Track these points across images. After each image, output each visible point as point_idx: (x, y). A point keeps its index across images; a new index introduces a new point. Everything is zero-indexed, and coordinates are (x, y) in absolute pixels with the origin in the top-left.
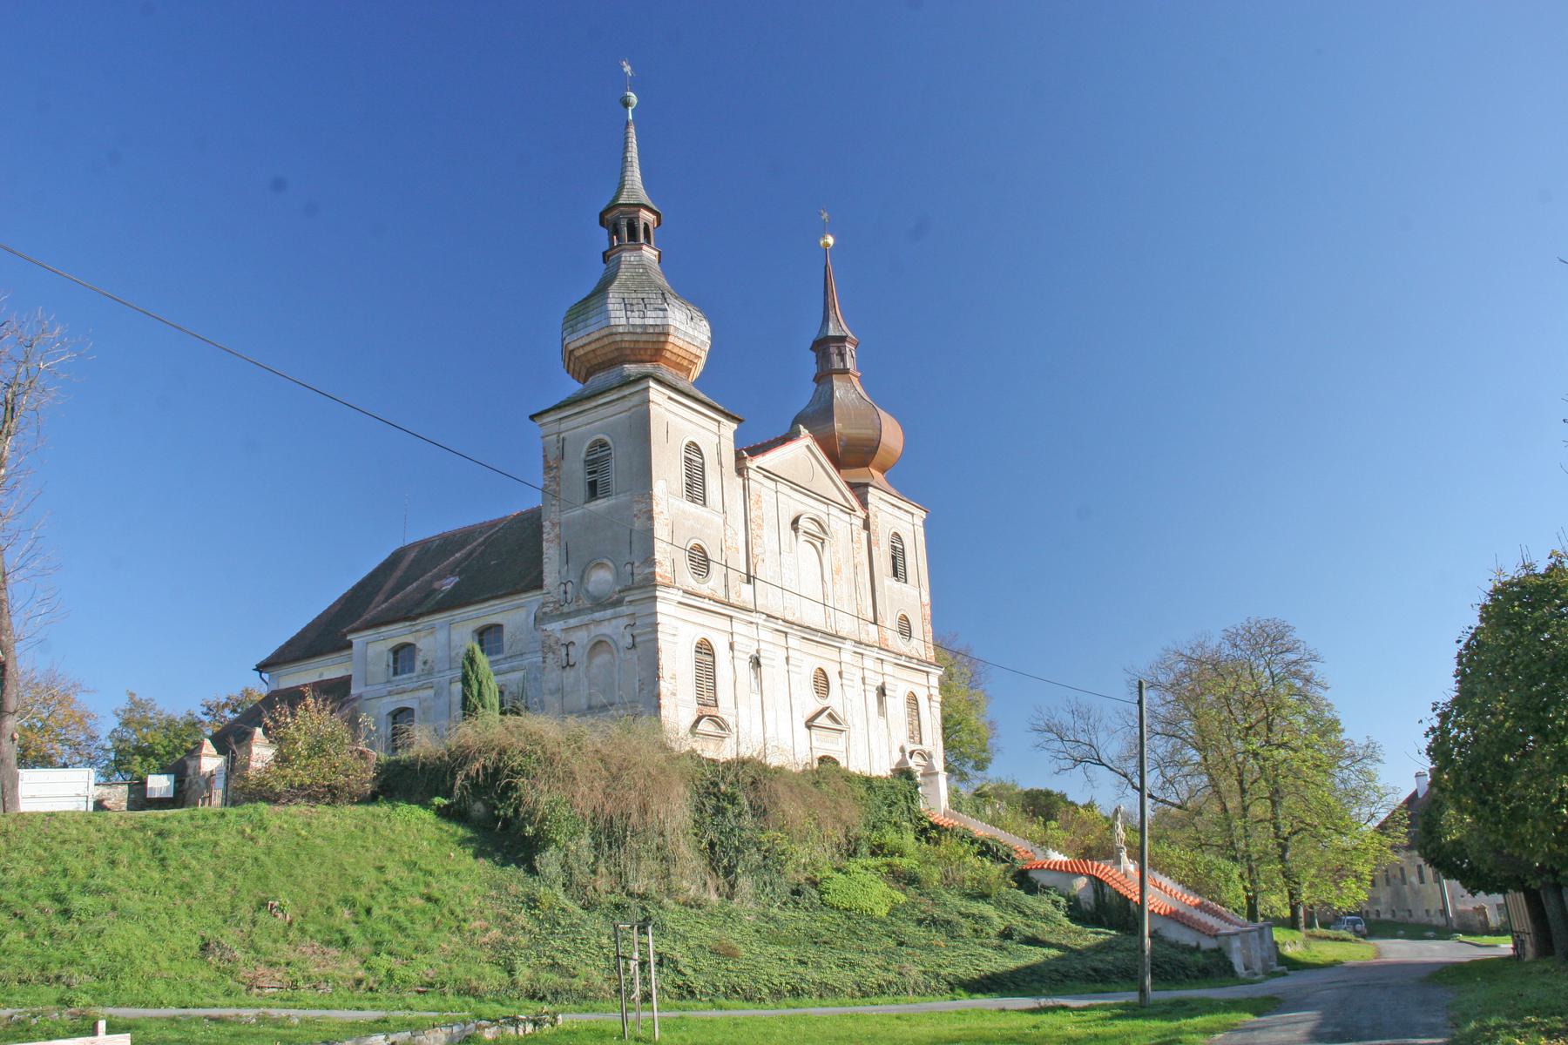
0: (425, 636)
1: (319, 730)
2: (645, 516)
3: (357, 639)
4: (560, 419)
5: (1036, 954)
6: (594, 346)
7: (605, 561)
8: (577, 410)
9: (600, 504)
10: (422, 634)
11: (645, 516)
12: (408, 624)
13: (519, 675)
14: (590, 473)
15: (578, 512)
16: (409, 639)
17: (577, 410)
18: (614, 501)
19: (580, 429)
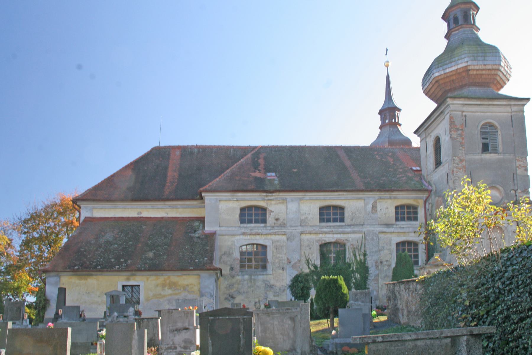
0: (275, 204)
1: (3, 224)
2: (523, 169)
3: (208, 197)
4: (466, 104)
5: (324, 324)
6: (484, 72)
7: (498, 186)
8: (479, 103)
9: (487, 156)
10: (273, 202)
11: (523, 169)
12: (265, 194)
13: (359, 236)
14: (483, 138)
15: (477, 157)
16: (262, 204)
17: (479, 103)
18: (502, 157)
19: (477, 114)
